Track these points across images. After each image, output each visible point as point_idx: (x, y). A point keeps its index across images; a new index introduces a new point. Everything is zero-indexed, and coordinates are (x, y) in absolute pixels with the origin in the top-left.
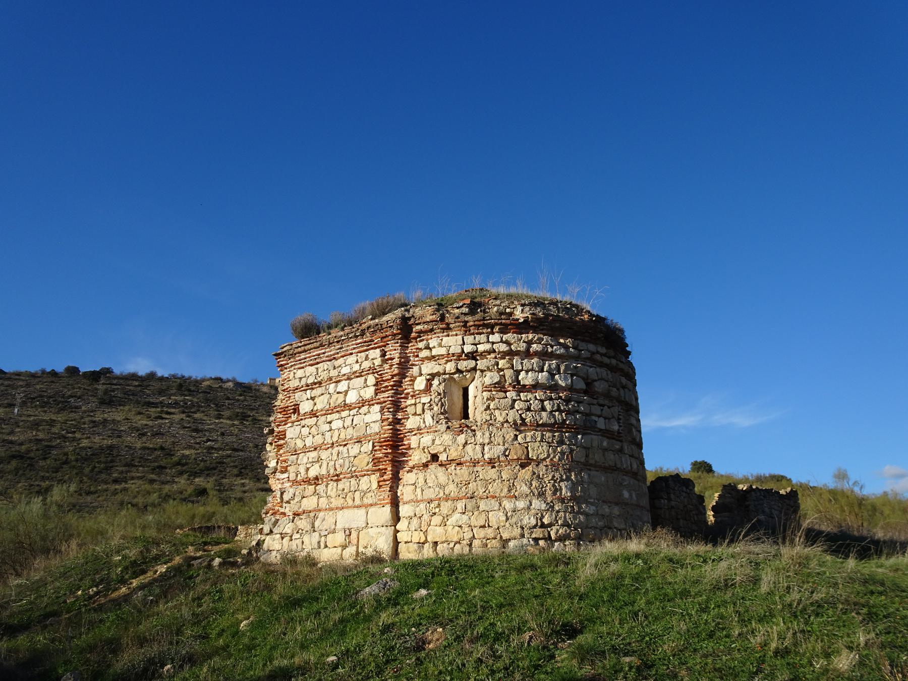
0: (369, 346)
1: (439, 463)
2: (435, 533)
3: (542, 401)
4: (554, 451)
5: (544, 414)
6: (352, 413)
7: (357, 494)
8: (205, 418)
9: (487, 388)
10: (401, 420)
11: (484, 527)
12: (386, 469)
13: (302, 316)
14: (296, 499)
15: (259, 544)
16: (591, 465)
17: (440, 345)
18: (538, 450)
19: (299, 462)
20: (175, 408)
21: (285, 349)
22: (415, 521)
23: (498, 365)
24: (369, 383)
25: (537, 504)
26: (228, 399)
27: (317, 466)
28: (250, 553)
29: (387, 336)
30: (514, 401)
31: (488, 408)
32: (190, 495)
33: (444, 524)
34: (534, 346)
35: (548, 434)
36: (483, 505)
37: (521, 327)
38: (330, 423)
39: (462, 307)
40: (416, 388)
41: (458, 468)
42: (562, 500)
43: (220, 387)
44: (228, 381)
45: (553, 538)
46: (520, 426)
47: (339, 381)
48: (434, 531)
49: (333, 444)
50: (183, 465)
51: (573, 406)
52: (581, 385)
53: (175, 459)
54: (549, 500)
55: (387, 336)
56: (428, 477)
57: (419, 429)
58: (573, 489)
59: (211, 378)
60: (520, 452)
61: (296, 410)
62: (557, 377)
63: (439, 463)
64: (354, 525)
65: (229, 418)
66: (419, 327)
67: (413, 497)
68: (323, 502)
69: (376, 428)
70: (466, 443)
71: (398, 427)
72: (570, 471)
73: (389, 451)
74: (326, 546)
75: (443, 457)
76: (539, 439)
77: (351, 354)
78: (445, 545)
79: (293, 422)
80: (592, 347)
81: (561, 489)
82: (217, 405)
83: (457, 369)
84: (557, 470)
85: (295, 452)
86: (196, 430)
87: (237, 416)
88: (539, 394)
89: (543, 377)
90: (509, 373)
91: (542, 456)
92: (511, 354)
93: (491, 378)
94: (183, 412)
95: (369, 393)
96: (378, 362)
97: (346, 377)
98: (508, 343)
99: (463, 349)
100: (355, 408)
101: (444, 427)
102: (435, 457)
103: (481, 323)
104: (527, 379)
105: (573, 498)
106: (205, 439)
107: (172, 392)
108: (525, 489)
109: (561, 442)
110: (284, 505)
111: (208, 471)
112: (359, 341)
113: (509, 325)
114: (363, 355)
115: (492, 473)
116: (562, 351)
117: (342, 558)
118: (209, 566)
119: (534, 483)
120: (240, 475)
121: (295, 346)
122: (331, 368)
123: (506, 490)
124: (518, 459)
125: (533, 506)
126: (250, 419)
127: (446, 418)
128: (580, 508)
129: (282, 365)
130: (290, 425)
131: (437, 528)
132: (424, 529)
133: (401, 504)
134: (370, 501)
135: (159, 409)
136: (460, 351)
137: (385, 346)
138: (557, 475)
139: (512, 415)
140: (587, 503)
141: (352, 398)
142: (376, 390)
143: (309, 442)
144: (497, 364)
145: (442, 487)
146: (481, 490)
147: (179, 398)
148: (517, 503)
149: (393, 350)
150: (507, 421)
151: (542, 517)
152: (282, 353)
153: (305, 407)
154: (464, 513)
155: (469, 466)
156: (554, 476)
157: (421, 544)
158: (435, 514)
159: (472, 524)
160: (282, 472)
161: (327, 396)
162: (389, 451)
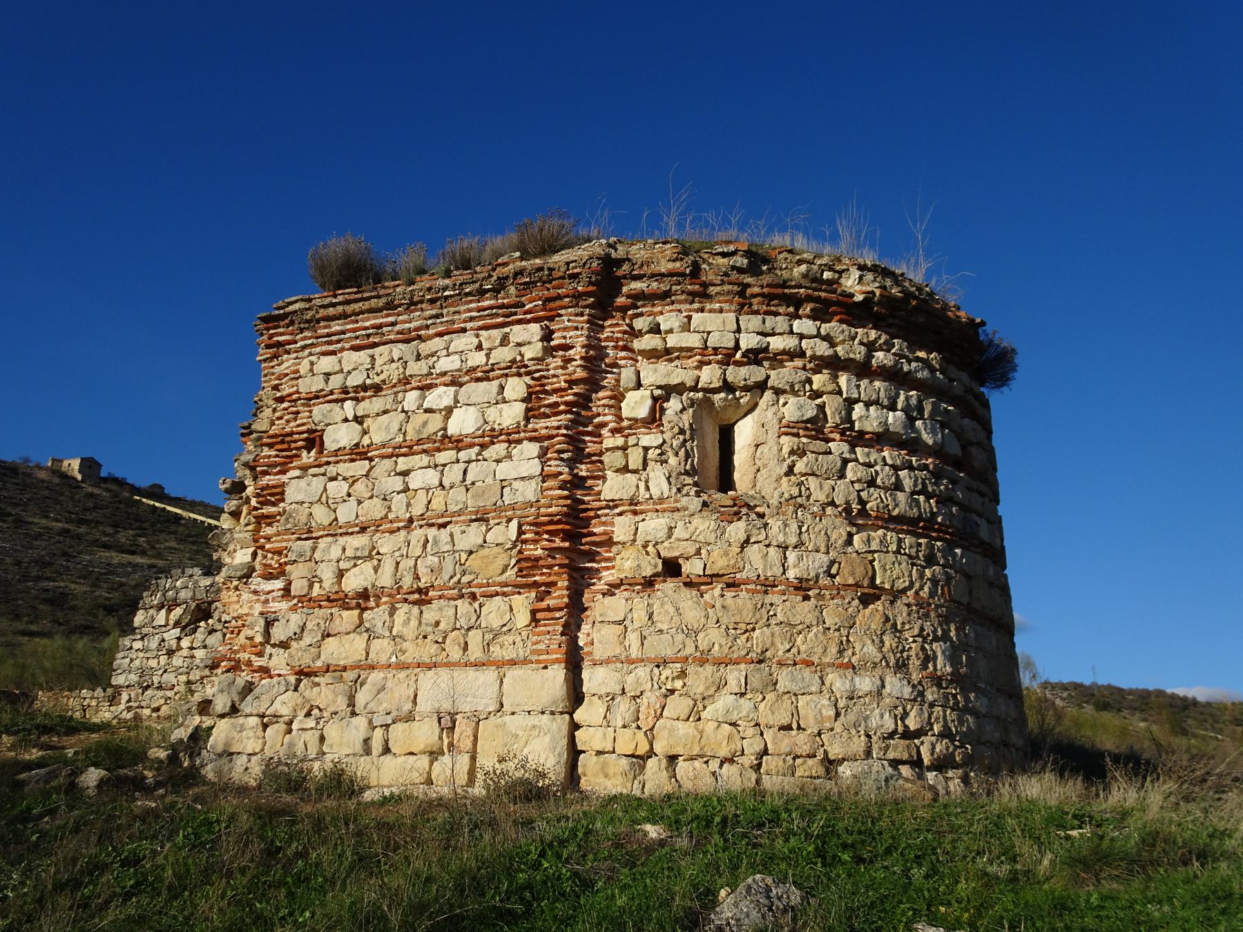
0: (510, 315)
1: (683, 578)
2: (674, 734)
3: (895, 468)
4: (922, 576)
5: (901, 496)
6: (463, 455)
7: (475, 638)
9: (790, 429)
10: (584, 479)
11: (788, 728)
12: (554, 584)
13: (337, 246)
14: (307, 639)
15: (199, 737)
17: (686, 327)
18: (891, 572)
19: (317, 556)
21: (291, 308)
22: (623, 708)
24: (508, 393)
25: (895, 686)
27: (367, 567)
28: (174, 759)
29: (559, 297)
30: (845, 462)
31: (790, 471)
33: (694, 715)
34: (880, 355)
35: (908, 540)
36: (785, 680)
38: (405, 474)
39: (734, 253)
40: (626, 412)
41: (729, 594)
42: (937, 681)
45: (926, 762)
47: (430, 387)
48: (672, 731)
49: (411, 521)
51: (946, 487)
52: (954, 449)
54: (915, 677)
55: (559, 297)
56: (656, 608)
57: (633, 502)
58: (953, 659)
60: (860, 571)
61: (314, 440)
62: (919, 423)
63: (683, 578)
64: (466, 706)
66: (637, 285)
68: (382, 650)
69: (528, 491)
70: (747, 541)
71: (579, 494)
73: (558, 543)
74: (387, 750)
75: (692, 568)
76: (894, 547)
77: (464, 330)
78: (697, 764)
79: (305, 469)
81: (935, 658)
83: (725, 380)
84: (927, 616)
85: (308, 534)
90: (832, 405)
91: (900, 585)
92: (834, 364)
93: (794, 408)
95: (511, 414)
96: (533, 351)
97: (447, 379)
99: (737, 341)
100: (471, 446)
101: (696, 503)
102: (672, 568)
103: (779, 291)
104: (868, 419)
105: (956, 679)
108: (871, 650)
109: (930, 560)
110: (268, 649)
112: (486, 303)
113: (829, 304)
114: (497, 334)
115: (804, 611)
117: (429, 782)
118: (72, 788)
121: (318, 302)
122: (410, 358)
123: (834, 650)
124: (857, 585)
125: (888, 689)
126: (10, 519)
127: (695, 484)
128: (967, 700)
129: (279, 344)
131: (680, 724)
132: (645, 724)
133: (586, 664)
134: (509, 654)
136: (731, 344)
137: (551, 319)
138: (928, 629)
139: (843, 492)
140: (977, 690)
142: (528, 410)
143: (346, 513)
144: (809, 381)
146: (782, 647)
148: (857, 680)
149: (573, 331)
150: (832, 503)
151: (906, 714)
152: (285, 316)
153: (340, 436)
154: (742, 695)
155: (754, 592)
156: (922, 629)
157: (640, 760)
158: (672, 691)
159: (762, 721)
160: (269, 577)
161: (396, 419)
162: (558, 543)
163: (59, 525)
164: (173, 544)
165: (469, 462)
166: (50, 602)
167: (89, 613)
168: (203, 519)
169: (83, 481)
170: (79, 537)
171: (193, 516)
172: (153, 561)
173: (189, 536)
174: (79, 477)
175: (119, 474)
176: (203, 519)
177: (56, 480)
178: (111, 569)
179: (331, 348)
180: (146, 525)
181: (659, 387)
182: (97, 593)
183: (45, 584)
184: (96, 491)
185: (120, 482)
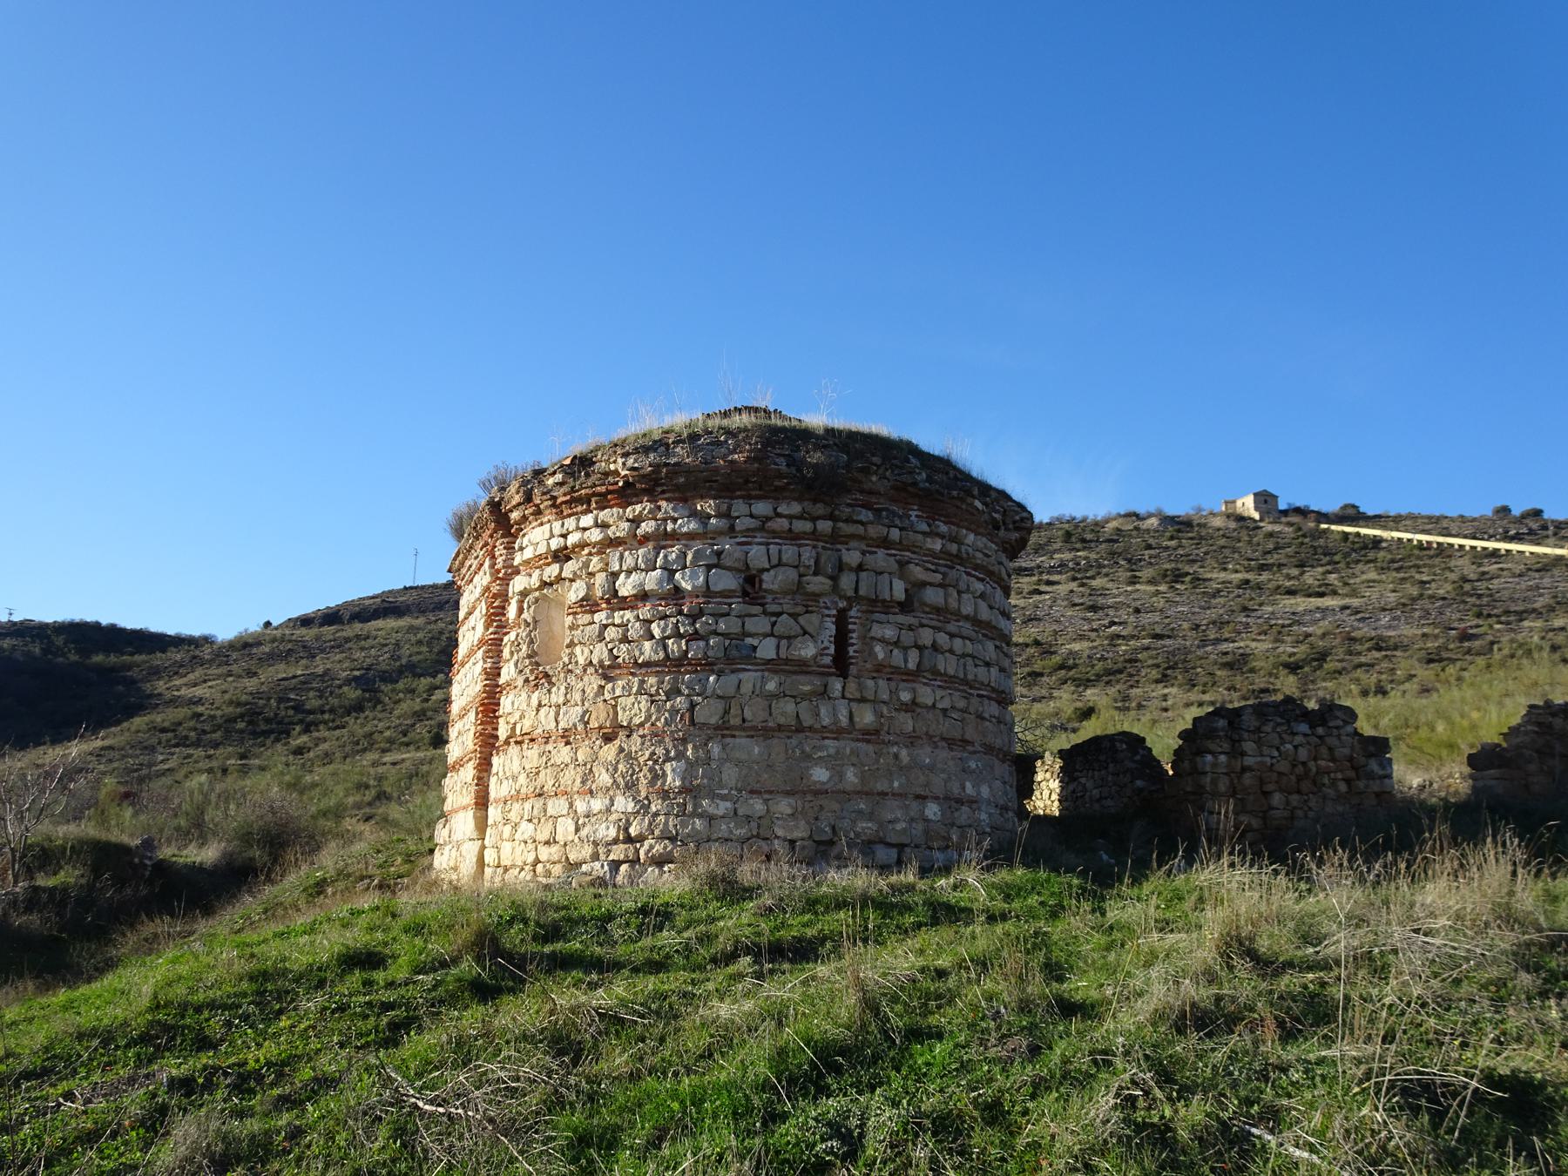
8: (1110, 585)
18: (633, 709)
20: (1060, 573)
25: (623, 804)
26: (1149, 547)
32: (1069, 720)
35: (652, 680)
37: (626, 494)
43: (1137, 528)
44: (1150, 515)
46: (607, 672)
50: (1070, 668)
53: (1056, 659)
59: (1120, 516)
60: (603, 715)
65: (1151, 582)
72: (684, 741)
80: (762, 508)
81: (664, 775)
82: (1129, 561)
84: (660, 742)
86: (1094, 608)
87: (1165, 576)
88: (645, 611)
89: (652, 580)
91: (637, 721)
94: (1074, 579)
98: (604, 526)
105: (684, 790)
106: (1106, 622)
107: (1056, 546)
111: (1108, 676)
115: (563, 754)
116: (693, 525)
117: (455, 869)
119: (621, 767)
120: (1164, 679)
123: (579, 780)
124: (600, 728)
126: (1188, 579)
128: (695, 806)
135: (1035, 578)
139: (600, 653)
140: (713, 796)
147: (1067, 556)
151: (628, 824)
163: (1239, 576)
164: (1373, 575)
166: (1229, 666)
167: (1270, 674)
168: (1409, 536)
169: (1262, 520)
170: (1259, 587)
171: (1396, 535)
172: (1347, 601)
173: (1393, 561)
174: (1257, 516)
175: (1300, 503)
176: (1409, 536)
177: (1233, 525)
178: (1296, 619)
180: (1337, 558)
182: (1281, 650)
183: (1225, 647)
184: (1277, 528)
185: (1298, 511)
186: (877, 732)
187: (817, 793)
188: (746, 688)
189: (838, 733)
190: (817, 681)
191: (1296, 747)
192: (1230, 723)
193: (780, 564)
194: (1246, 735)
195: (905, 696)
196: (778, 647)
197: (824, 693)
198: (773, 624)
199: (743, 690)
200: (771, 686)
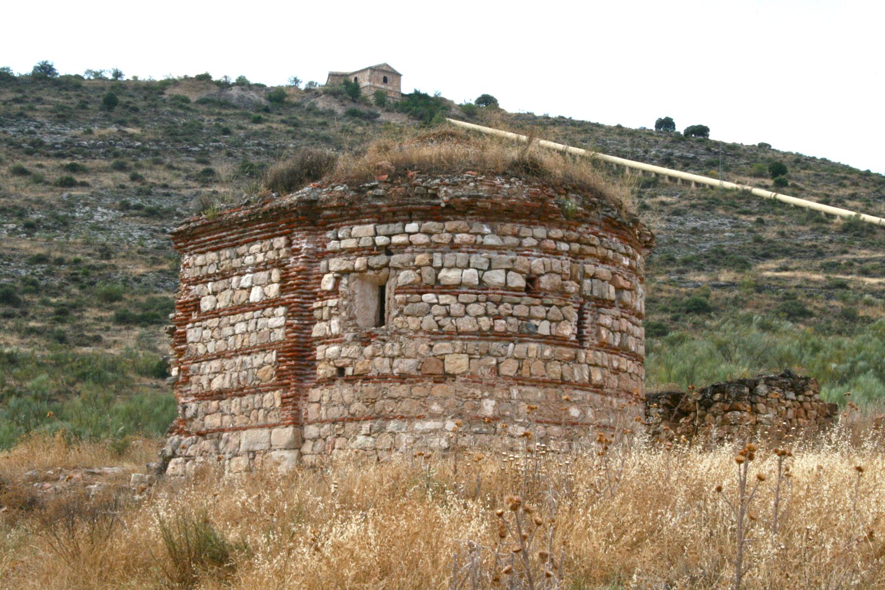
16: (524, 379)
17: (350, 237)
23: (414, 261)
27: (220, 376)
38: (233, 325)
61: (196, 304)
67: (317, 416)
69: (279, 335)
75: (349, 371)
79: (194, 322)
80: (540, 232)
89: (470, 275)
94: (121, 167)
95: (273, 290)
96: (283, 253)
99: (374, 241)
100: (258, 309)
112: (262, 225)
129: (180, 247)
130: (190, 325)
141: (256, 295)
143: (211, 347)
145: (348, 406)
153: (206, 304)
154: (369, 435)
161: (229, 293)
165: (258, 318)
179: (202, 249)
181: (337, 272)
186: (601, 387)
187: (573, 424)
188: (532, 354)
189: (582, 386)
190: (572, 351)
191: (787, 408)
192: (751, 390)
193: (552, 272)
194: (759, 399)
195: (615, 364)
196: (550, 327)
197: (575, 359)
198: (547, 312)
199: (530, 355)
200: (547, 353)
